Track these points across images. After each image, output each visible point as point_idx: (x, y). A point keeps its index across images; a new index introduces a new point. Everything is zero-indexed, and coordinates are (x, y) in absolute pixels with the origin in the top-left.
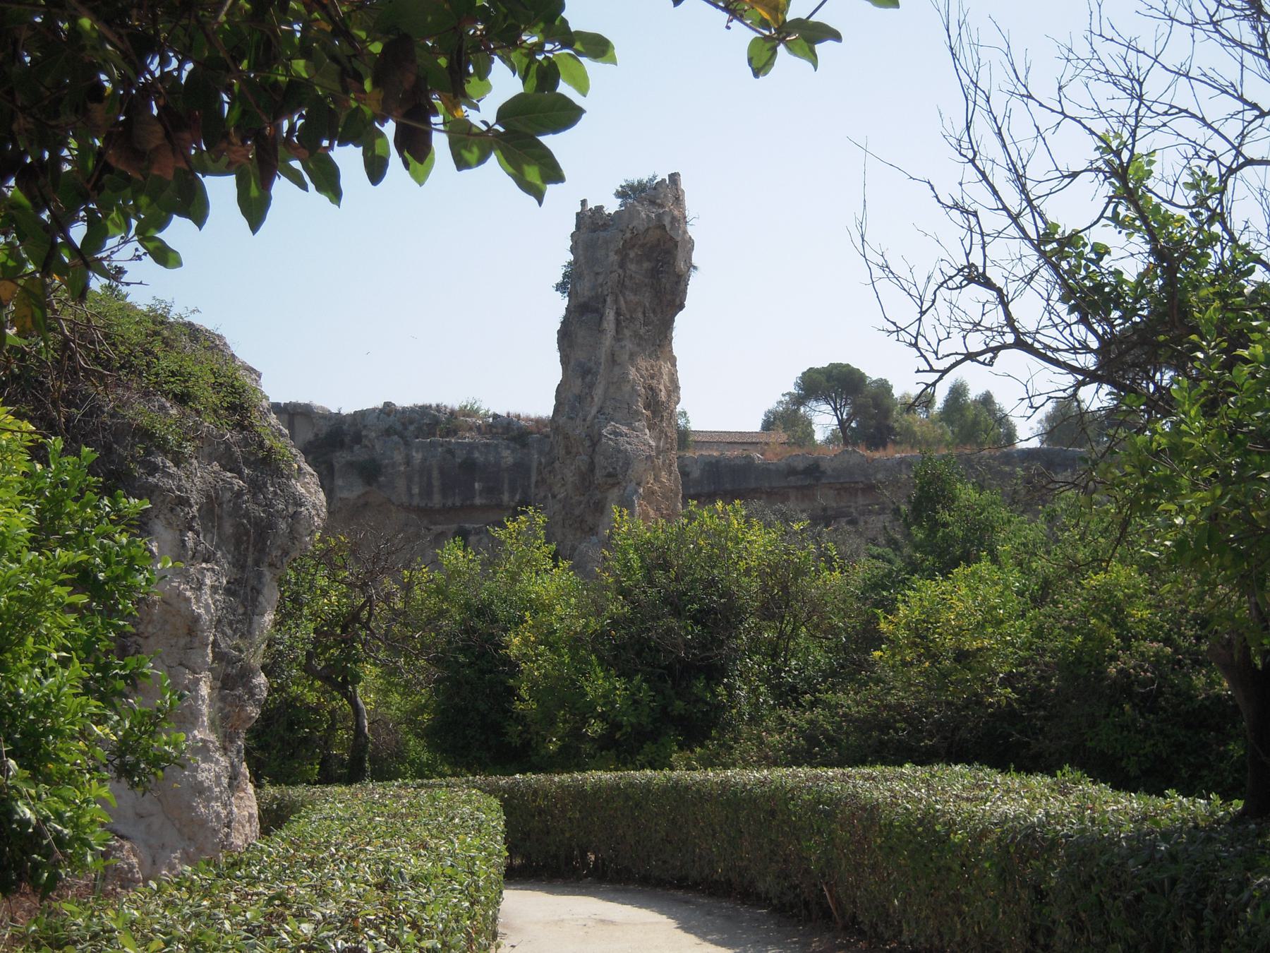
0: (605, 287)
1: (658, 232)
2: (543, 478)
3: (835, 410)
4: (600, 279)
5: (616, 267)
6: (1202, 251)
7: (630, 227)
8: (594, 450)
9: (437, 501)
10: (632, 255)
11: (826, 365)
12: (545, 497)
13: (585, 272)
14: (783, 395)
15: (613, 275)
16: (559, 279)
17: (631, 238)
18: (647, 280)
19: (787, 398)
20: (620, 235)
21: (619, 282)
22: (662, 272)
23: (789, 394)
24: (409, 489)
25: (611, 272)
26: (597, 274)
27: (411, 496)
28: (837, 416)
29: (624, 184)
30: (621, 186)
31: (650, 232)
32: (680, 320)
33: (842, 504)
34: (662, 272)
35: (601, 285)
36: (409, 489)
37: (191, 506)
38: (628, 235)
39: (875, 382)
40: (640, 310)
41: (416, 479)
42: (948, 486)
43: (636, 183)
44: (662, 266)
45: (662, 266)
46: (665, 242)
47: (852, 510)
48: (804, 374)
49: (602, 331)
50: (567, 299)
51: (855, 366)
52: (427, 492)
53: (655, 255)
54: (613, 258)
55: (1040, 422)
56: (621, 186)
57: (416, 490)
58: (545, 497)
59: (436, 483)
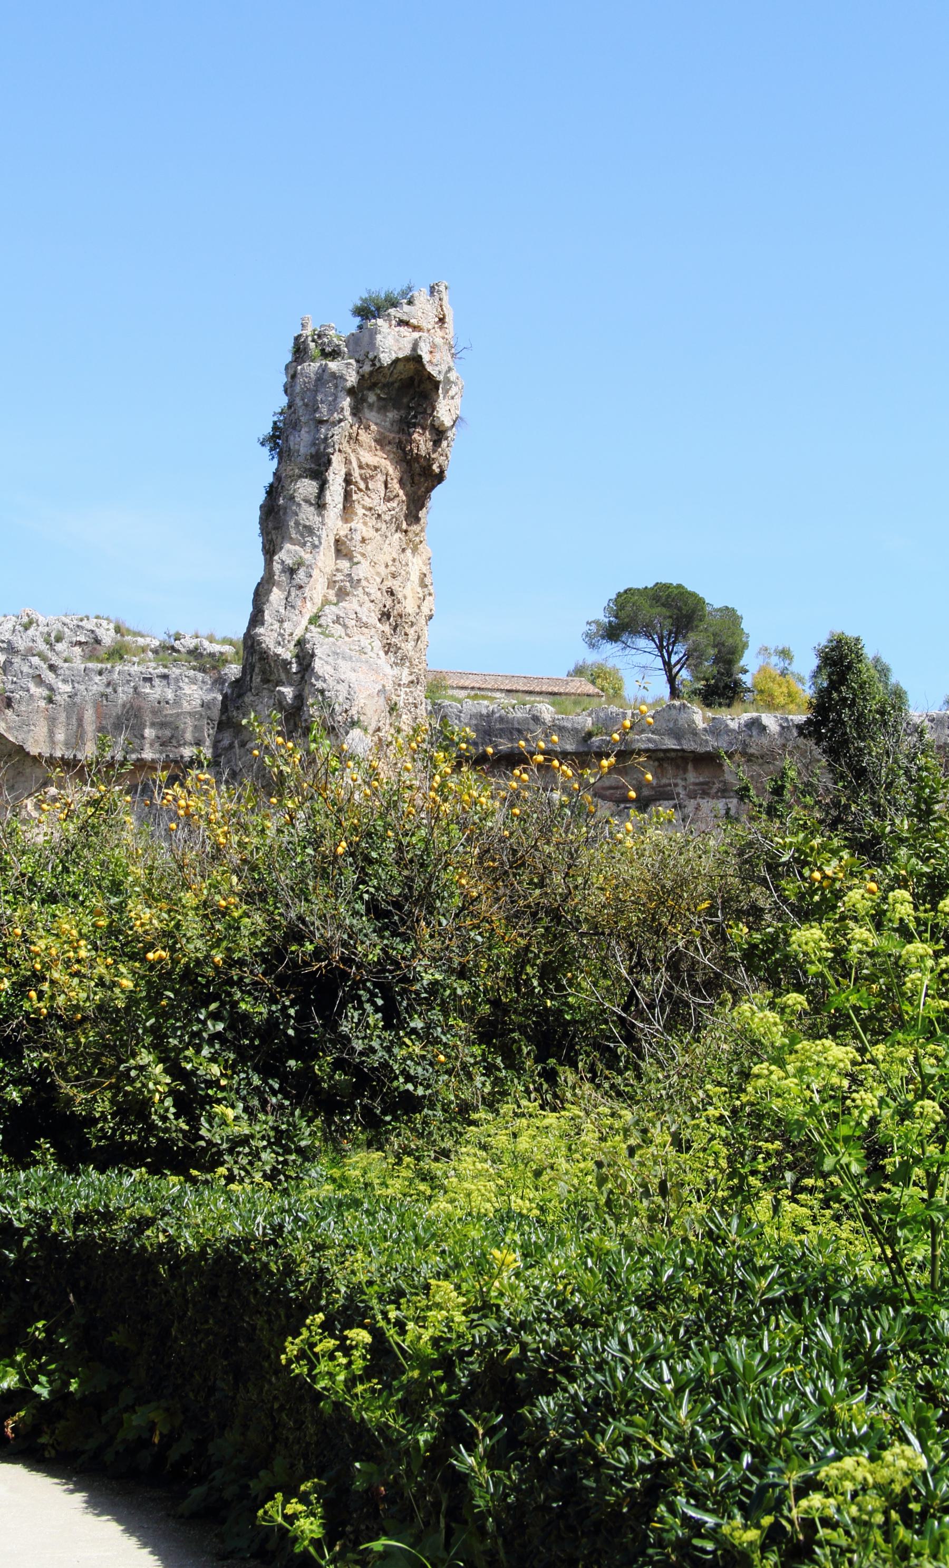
1: (411, 366)
2: (229, 718)
3: (660, 648)
7: (371, 356)
8: (303, 678)
9: (89, 751)
10: (372, 398)
11: (650, 585)
12: (231, 746)
14: (589, 623)
16: (268, 430)
17: (371, 373)
18: (392, 436)
19: (594, 627)
23: (597, 622)
24: (51, 734)
27: (52, 742)
28: (662, 656)
30: (361, 299)
31: (400, 366)
33: (664, 781)
36: (51, 734)
39: (720, 610)
40: (381, 478)
41: (62, 717)
42: (841, 1065)
43: (383, 296)
44: (415, 417)
47: (680, 790)
48: (619, 595)
50: (276, 460)
51: (690, 588)
52: (77, 739)
53: (405, 400)
56: (361, 299)
57: (60, 737)
58: (231, 746)
59: (90, 727)
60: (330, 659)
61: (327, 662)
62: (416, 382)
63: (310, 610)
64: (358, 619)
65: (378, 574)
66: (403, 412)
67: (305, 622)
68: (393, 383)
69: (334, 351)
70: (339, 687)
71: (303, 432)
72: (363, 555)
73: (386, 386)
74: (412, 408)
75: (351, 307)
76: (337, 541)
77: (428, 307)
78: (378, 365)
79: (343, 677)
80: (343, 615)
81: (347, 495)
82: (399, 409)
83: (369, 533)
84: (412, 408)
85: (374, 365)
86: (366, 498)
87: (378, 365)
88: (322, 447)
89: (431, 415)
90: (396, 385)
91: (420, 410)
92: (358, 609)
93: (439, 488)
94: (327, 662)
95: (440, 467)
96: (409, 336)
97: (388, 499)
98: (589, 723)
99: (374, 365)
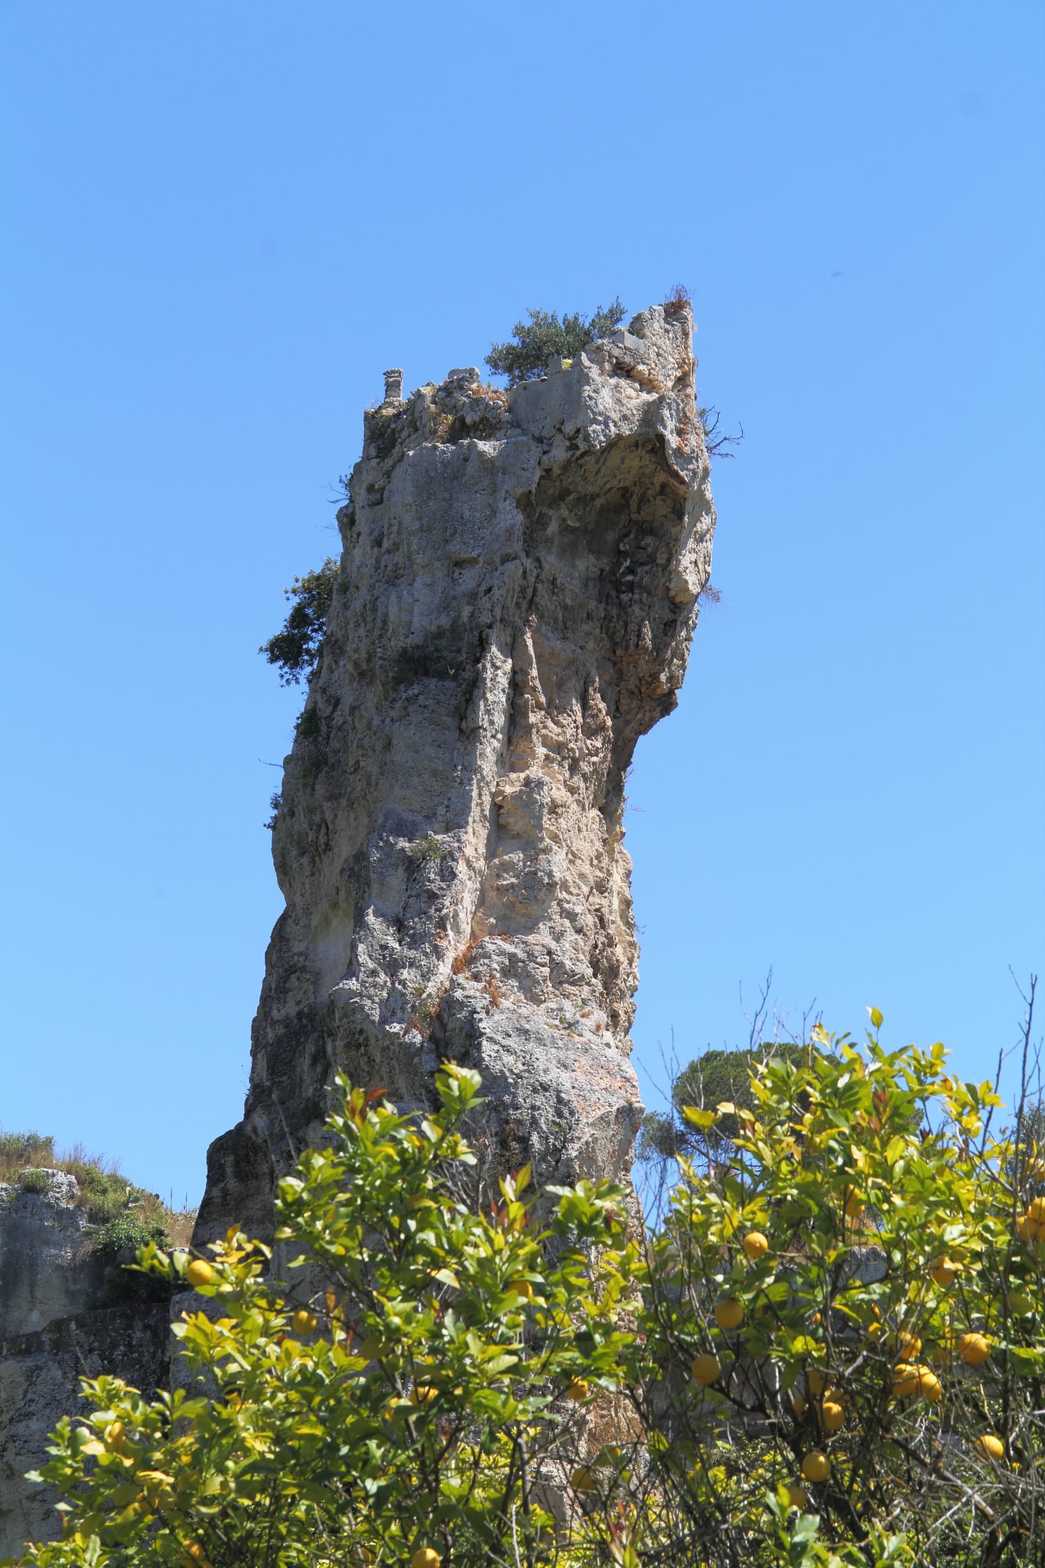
0: (484, 602)
1: (636, 461)
4: (468, 579)
5: (518, 546)
6: (400, 1232)
7: (569, 428)
13: (419, 559)
15: (510, 566)
17: (566, 467)
20: (536, 450)
21: (523, 590)
22: (631, 587)
25: (506, 559)
26: (459, 564)
29: (528, 323)
31: (614, 459)
32: (206, 1173)
34: (631, 587)
35: (473, 597)
37: (1013, 1504)
38: (559, 453)
44: (630, 571)
45: (630, 571)
46: (643, 500)
49: (470, 734)
53: (611, 537)
54: (511, 517)
55: (203, 1407)
56: (519, 331)
60: (512, 1042)
61: (507, 1049)
62: (634, 503)
63: (454, 946)
64: (556, 967)
65: (582, 876)
66: (605, 563)
67: (444, 969)
68: (594, 497)
69: (483, 420)
70: (539, 1100)
71: (419, 583)
72: (555, 838)
73: (584, 500)
74: (624, 554)
75: (488, 352)
76: (497, 807)
77: (666, 344)
78: (583, 447)
79: (544, 1079)
80: (521, 955)
81: (516, 714)
82: (598, 553)
83: (560, 794)
84: (624, 554)
85: (574, 447)
86: (550, 723)
87: (583, 447)
88: (466, 611)
89: (665, 567)
90: (599, 502)
91: (641, 556)
92: (553, 945)
93: (663, 725)
94: (507, 1049)
95: (671, 679)
96: (635, 398)
97: (590, 732)
98: (532, 1399)
99: (574, 447)
